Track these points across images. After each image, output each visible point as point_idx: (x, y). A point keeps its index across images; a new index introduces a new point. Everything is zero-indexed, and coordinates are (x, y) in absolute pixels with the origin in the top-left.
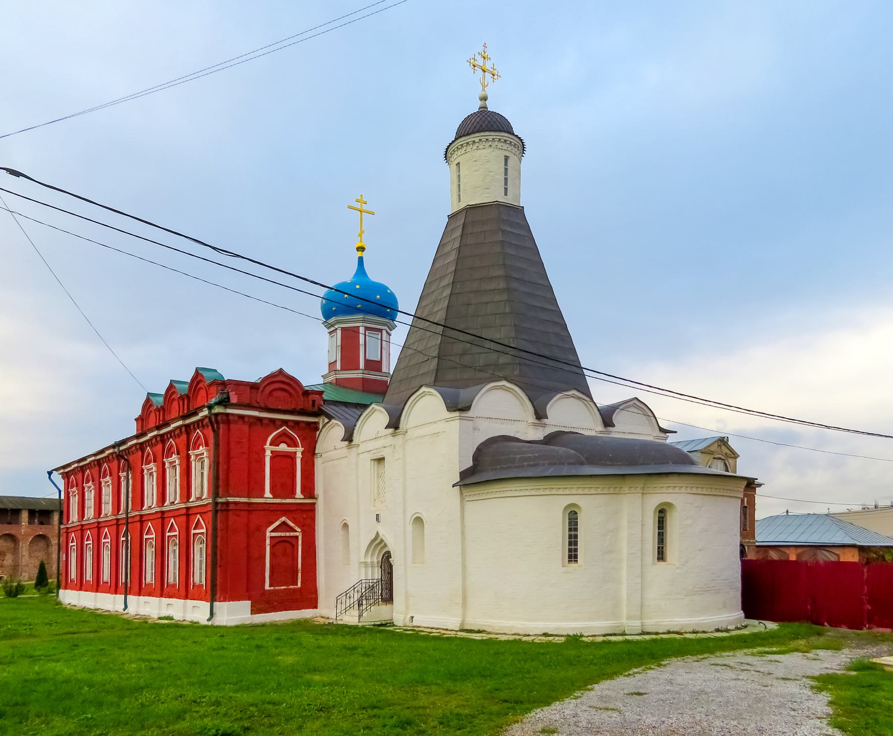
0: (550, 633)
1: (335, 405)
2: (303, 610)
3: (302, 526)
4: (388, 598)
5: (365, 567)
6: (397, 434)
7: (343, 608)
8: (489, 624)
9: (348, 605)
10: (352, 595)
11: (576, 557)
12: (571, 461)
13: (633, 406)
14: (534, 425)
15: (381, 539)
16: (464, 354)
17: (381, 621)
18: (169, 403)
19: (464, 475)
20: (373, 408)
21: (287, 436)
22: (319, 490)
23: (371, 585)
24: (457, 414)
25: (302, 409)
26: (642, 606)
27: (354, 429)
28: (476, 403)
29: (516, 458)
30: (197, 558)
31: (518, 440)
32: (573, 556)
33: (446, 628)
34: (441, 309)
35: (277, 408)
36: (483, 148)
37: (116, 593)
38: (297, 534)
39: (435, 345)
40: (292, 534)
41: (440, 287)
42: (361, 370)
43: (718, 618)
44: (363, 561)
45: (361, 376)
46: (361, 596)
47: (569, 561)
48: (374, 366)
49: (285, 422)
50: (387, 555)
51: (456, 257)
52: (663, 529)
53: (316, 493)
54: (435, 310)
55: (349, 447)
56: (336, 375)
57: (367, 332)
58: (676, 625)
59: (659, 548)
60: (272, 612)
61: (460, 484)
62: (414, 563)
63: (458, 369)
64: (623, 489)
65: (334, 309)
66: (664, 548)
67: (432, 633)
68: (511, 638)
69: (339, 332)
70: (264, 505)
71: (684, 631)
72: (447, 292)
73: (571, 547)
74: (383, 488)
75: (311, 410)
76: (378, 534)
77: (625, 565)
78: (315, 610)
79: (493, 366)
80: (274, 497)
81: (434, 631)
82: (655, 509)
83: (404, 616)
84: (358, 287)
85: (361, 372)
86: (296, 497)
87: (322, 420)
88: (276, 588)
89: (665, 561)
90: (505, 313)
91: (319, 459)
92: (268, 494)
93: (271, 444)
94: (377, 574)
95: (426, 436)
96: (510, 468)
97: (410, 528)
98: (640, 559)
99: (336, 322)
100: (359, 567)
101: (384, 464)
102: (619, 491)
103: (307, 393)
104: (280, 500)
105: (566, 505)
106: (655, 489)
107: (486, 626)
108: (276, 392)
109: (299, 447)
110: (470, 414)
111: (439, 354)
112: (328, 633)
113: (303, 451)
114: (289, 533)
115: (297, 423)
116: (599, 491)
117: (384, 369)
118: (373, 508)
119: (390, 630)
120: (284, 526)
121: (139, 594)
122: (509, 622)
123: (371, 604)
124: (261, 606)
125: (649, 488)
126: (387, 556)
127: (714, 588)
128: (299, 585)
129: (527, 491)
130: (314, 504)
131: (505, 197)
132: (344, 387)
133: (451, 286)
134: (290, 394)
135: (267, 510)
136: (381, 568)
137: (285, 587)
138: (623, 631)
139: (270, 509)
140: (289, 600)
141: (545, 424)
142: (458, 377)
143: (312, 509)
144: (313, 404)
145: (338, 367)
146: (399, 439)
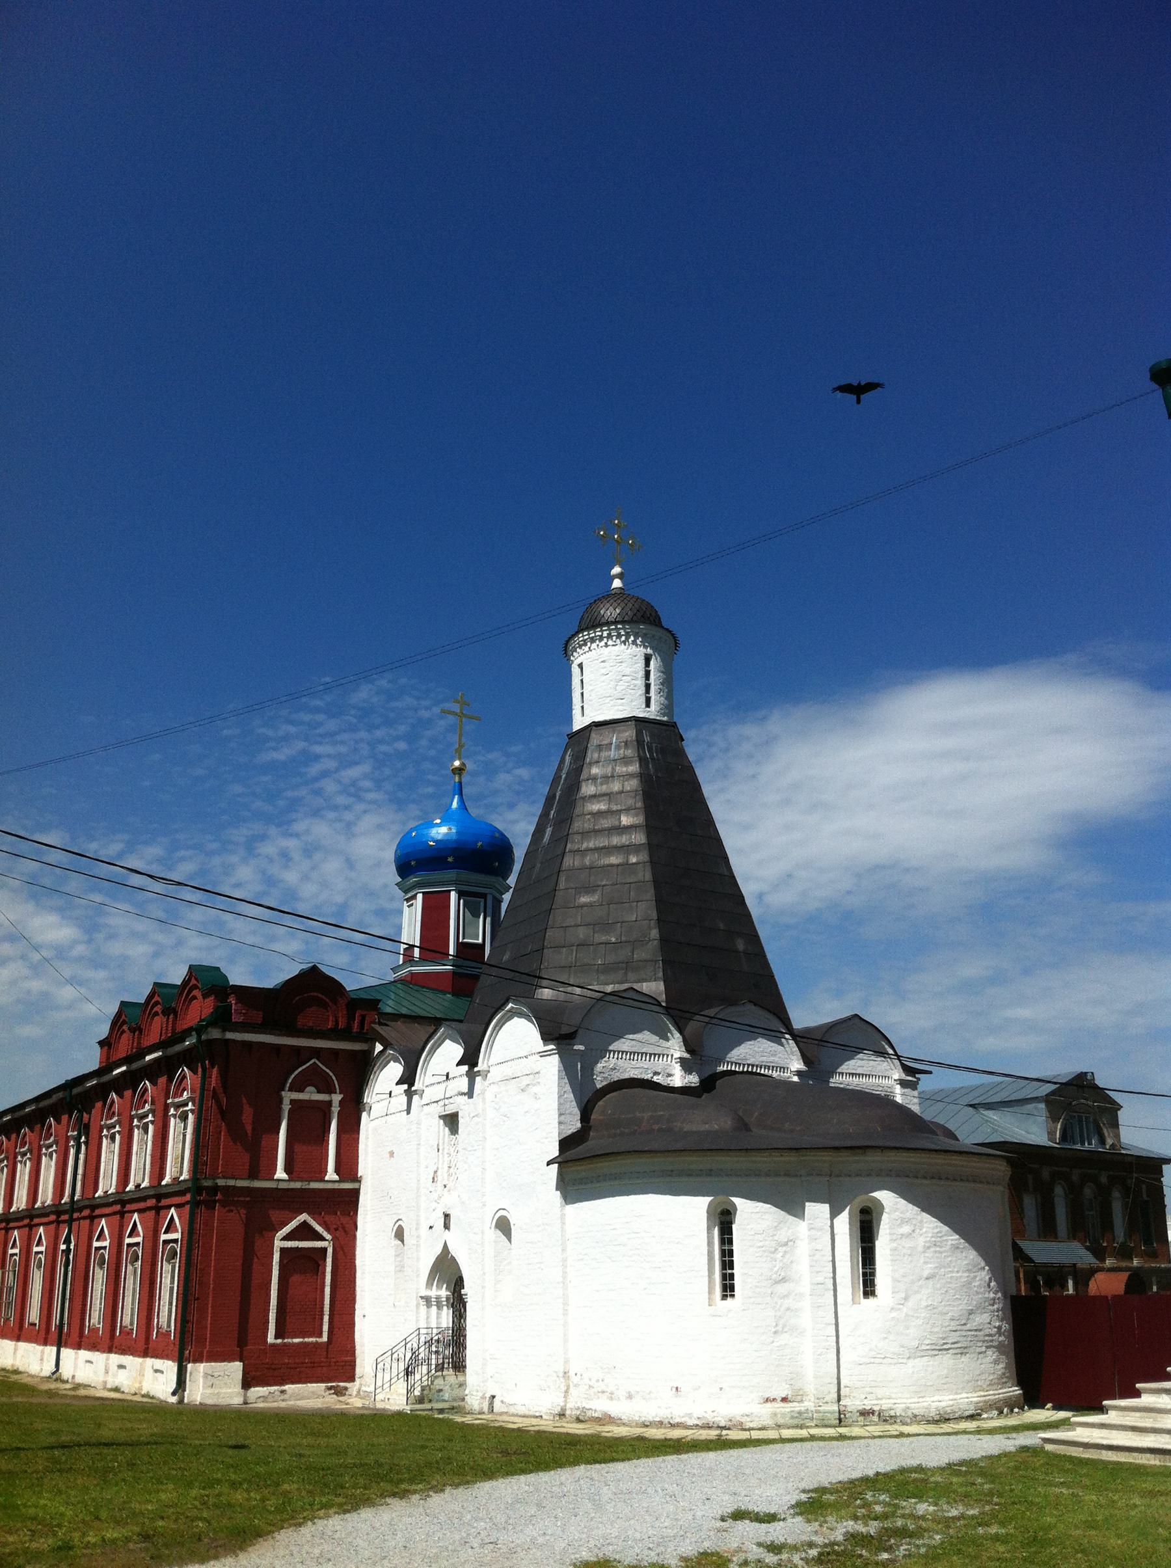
7: (387, 1378)
11: (732, 1288)
18: (149, 1020)
30: (167, 1281)
36: (613, 645)
37: (45, 1343)
49: (316, 1053)
61: (559, 1160)
69: (420, 896)
92: (280, 1174)
100: (418, 1305)
115: (335, 1053)
120: (304, 1232)
121: (78, 1346)
131: (648, 709)
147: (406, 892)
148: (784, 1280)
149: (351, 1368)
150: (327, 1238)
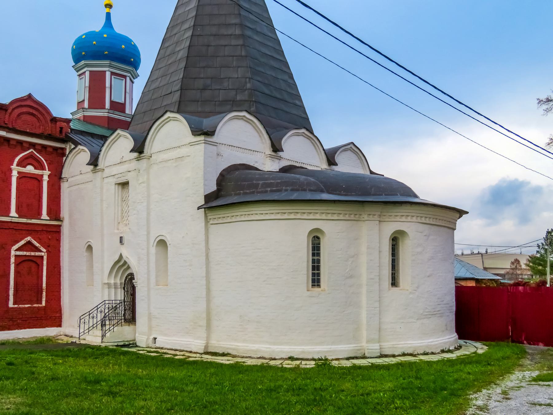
0: (295, 357)
1: (82, 135)
2: (47, 328)
3: (47, 247)
4: (131, 319)
5: (115, 288)
6: (141, 158)
7: (87, 327)
8: (234, 347)
9: (91, 324)
10: (95, 315)
11: (319, 281)
12: (312, 188)
13: (350, 150)
14: (271, 156)
15: (125, 261)
16: (205, 89)
17: (124, 341)
19: (208, 198)
20: (119, 133)
21: (34, 159)
22: (65, 213)
23: (114, 305)
24: (202, 138)
25: (49, 135)
26: (380, 330)
27: (99, 154)
28: (220, 130)
29: (259, 183)
31: (257, 169)
32: (316, 281)
33: (189, 350)
34: (183, 49)
35: (25, 130)
38: (43, 254)
39: (178, 80)
40: (37, 254)
41: (181, 30)
42: (107, 109)
43: (443, 340)
44: (106, 281)
45: (106, 115)
46: (104, 317)
47: (312, 285)
48: (118, 107)
49: (33, 145)
50: (130, 277)
51: (196, 5)
52: (395, 257)
53: (61, 216)
54: (178, 49)
55: (94, 171)
56: (84, 113)
57: (113, 77)
58: (410, 347)
59: (392, 273)
60: (15, 329)
62: (157, 285)
63: (199, 103)
64: (362, 217)
65: (83, 53)
66: (396, 274)
67: (177, 355)
68: (259, 362)
69: (87, 74)
70: (10, 224)
71: (417, 353)
72: (189, 33)
73: (318, 272)
74: (127, 211)
75: (58, 136)
76: (121, 256)
77: (364, 290)
78: (59, 328)
79: (232, 102)
80: (20, 217)
81: (178, 353)
82: (391, 236)
83: (147, 337)
84: (105, 36)
85: (107, 111)
86: (42, 218)
87: (68, 147)
88: (20, 306)
89: (396, 287)
90: (241, 56)
91: (65, 183)
92: (13, 213)
93: (18, 165)
94: (120, 295)
95: (170, 160)
96: (253, 193)
97: (153, 250)
98: (378, 284)
99: (85, 65)
100: (103, 288)
101: (128, 189)
102: (359, 218)
103: (55, 120)
104: (26, 220)
105: (309, 230)
106: (391, 217)
107: (231, 349)
108: (24, 115)
109: (46, 170)
110: (214, 139)
111: (181, 88)
112: (70, 354)
113: (50, 174)
114: (34, 253)
115: (44, 147)
116: (341, 217)
117: (127, 111)
118: (116, 231)
119: (133, 352)
120: (29, 246)
122: (254, 345)
123: (114, 325)
124: (4, 324)
125: (385, 216)
126: (130, 278)
127: (440, 312)
128: (44, 304)
129: (267, 215)
130: (60, 226)
132: (91, 123)
133: (192, 28)
134: (38, 119)
135: (13, 229)
136: (124, 289)
137: (29, 305)
138: (363, 354)
139: (15, 228)
140: (34, 318)
141: (280, 157)
142: (200, 109)
143: (58, 230)
144: (61, 132)
145: (86, 105)
146: (144, 163)
147: (77, 71)
148: (351, 277)
149: (59, 320)
150: (43, 251)
